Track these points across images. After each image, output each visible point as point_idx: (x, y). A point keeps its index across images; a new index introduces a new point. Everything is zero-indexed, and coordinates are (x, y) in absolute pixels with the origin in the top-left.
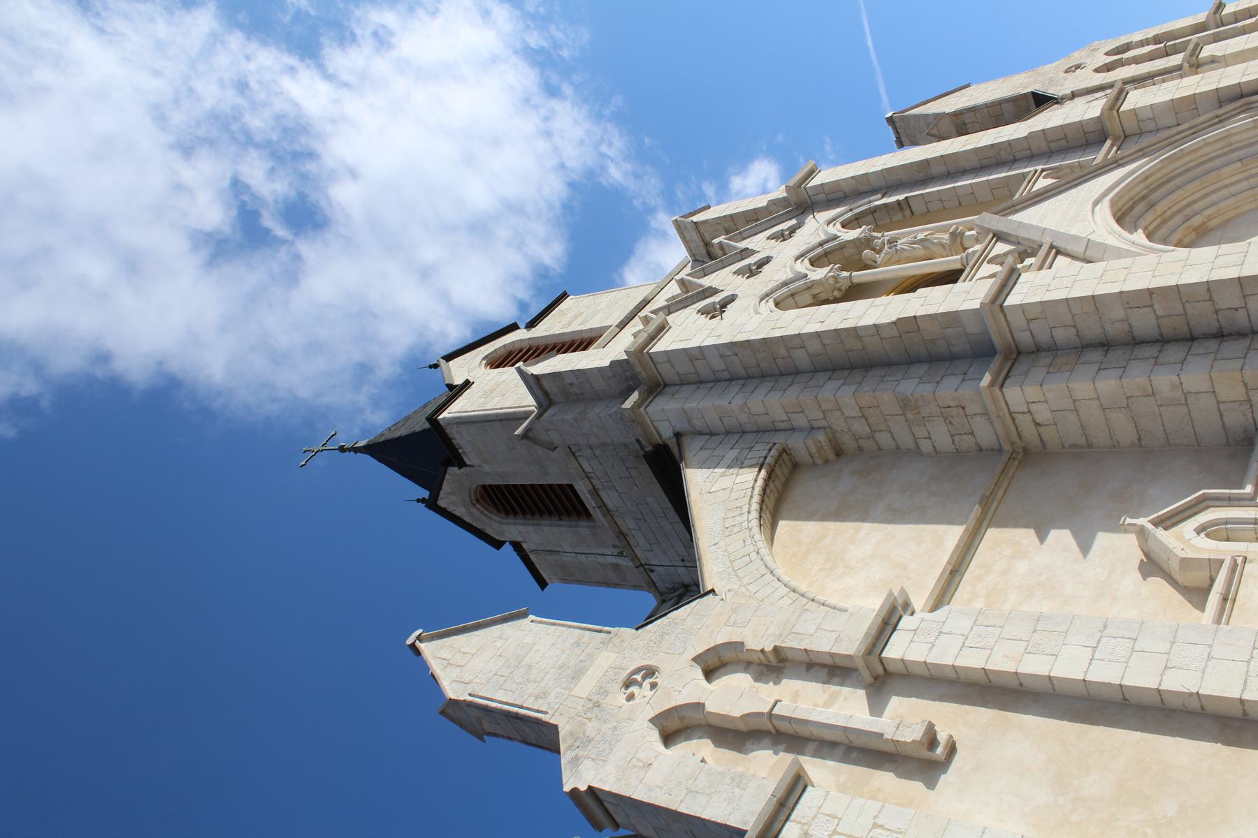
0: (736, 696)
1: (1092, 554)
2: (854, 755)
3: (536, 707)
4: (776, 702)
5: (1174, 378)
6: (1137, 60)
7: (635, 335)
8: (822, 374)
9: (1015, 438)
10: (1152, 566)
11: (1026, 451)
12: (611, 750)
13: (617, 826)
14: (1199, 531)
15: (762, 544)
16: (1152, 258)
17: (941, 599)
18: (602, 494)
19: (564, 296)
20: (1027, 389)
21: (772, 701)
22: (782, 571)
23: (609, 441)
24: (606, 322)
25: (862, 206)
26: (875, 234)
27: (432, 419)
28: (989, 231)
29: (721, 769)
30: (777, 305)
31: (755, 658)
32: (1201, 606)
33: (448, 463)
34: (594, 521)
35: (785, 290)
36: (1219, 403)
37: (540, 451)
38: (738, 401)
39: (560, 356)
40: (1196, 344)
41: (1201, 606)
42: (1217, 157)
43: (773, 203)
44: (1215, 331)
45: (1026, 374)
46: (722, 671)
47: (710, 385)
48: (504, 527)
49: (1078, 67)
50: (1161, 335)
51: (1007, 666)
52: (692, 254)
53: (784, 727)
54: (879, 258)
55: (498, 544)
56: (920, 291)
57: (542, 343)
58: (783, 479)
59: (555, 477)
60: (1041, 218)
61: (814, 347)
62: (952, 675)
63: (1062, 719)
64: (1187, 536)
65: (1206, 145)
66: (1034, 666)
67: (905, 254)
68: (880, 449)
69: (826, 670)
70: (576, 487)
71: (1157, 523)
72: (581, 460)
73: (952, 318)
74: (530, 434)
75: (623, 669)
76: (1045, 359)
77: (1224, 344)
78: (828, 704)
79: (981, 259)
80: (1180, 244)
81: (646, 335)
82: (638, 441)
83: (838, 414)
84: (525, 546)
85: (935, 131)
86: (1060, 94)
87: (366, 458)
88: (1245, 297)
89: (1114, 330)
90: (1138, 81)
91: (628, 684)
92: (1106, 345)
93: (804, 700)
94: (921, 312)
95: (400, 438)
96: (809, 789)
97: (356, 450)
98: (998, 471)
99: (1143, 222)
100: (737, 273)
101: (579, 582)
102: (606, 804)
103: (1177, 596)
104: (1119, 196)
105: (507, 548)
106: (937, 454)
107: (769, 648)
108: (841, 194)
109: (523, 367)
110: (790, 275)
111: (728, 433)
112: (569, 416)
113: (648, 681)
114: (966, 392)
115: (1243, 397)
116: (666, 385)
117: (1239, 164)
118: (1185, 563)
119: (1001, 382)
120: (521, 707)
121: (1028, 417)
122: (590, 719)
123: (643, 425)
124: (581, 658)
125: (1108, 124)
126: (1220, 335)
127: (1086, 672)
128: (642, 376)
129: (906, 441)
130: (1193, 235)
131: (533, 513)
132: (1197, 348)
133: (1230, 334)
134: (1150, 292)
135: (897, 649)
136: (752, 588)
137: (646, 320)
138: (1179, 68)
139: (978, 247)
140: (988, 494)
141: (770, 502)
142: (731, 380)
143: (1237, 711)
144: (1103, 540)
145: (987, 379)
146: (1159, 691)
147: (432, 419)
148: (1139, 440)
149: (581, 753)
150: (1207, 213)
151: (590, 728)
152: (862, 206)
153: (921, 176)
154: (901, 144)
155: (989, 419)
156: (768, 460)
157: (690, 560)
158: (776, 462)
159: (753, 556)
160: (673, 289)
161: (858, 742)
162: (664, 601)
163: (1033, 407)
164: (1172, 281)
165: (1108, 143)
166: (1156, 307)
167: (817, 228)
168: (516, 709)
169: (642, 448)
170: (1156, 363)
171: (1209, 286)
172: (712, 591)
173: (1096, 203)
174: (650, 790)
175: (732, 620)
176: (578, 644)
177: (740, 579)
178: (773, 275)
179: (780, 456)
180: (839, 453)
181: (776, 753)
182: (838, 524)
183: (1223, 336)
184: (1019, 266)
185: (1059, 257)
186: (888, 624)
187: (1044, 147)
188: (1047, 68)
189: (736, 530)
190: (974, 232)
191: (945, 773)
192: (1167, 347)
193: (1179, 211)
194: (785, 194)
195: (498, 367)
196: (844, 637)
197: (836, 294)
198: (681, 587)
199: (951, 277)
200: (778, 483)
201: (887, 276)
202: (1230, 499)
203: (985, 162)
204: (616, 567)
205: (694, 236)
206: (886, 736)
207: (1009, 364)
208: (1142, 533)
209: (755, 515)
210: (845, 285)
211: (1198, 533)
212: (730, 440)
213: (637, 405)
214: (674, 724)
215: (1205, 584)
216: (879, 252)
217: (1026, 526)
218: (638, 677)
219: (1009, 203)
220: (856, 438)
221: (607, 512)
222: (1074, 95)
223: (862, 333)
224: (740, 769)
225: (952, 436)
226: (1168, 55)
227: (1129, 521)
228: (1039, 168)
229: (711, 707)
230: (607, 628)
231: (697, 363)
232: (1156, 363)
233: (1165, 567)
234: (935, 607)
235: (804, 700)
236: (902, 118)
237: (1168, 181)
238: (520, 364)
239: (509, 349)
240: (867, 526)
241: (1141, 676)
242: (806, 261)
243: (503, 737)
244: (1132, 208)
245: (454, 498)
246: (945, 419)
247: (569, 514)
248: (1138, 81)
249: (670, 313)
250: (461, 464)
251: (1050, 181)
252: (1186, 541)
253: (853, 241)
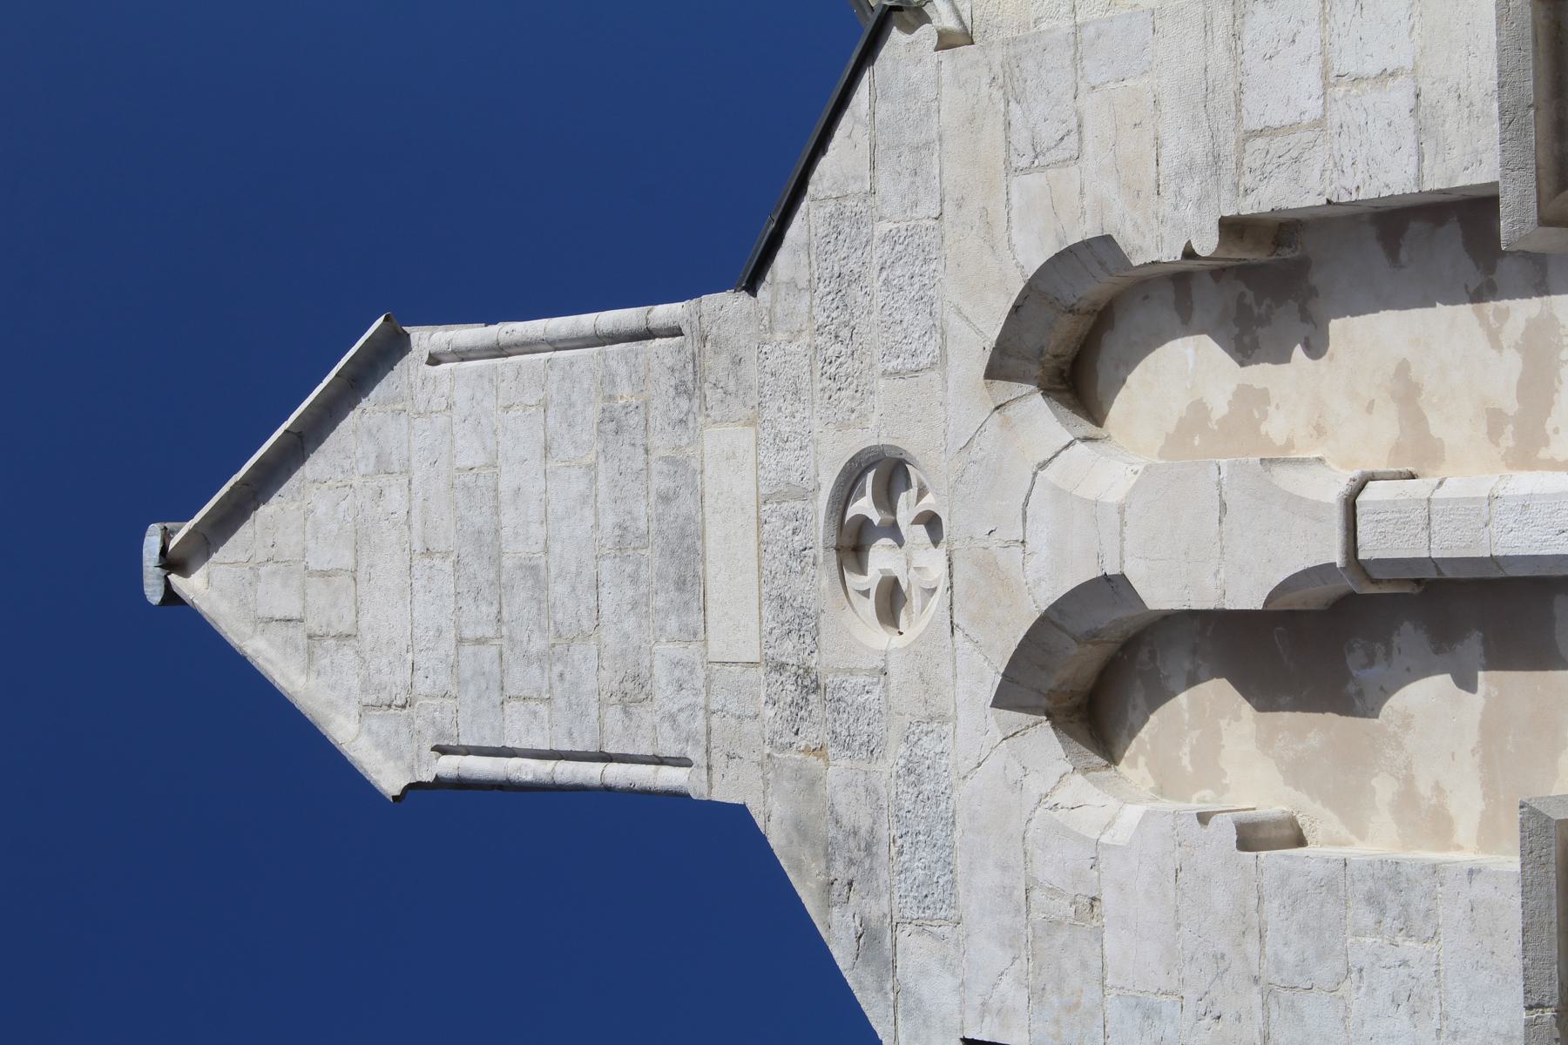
0: (1212, 477)
4: (1350, 506)
46: (1112, 345)
149: (876, 909)
175: (1021, 139)
218: (864, 506)
230: (663, 313)
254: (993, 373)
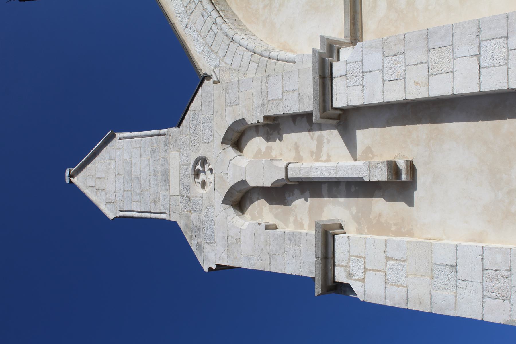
46: (244, 138)
63: (477, 120)
91: (197, 174)
124: (161, 162)
136: (228, 60)
149: (200, 240)
175: (228, 101)
191: (415, 190)
218: (199, 167)
254: (222, 143)
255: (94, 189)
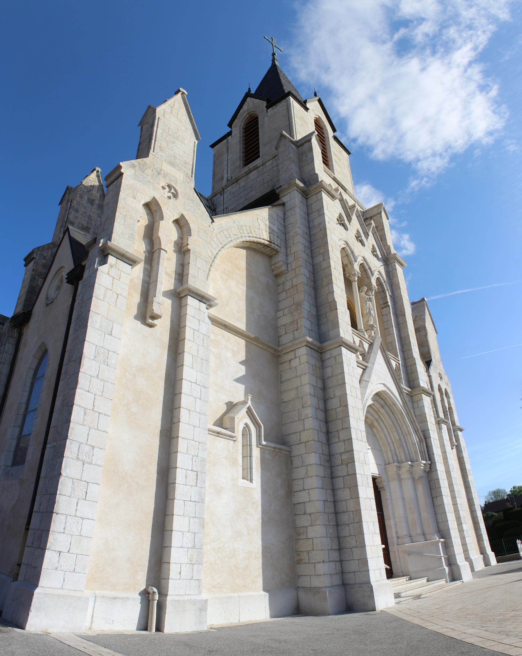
0: (168, 234)
1: (235, 383)
2: (146, 285)
3: (156, 147)
5: (310, 415)
6: (442, 400)
7: (330, 185)
8: (312, 269)
9: (284, 352)
10: (231, 406)
11: (279, 356)
12: (140, 181)
13: (108, 187)
14: (246, 424)
15: (235, 243)
16: (360, 406)
17: (216, 322)
18: (256, 171)
19: (349, 153)
20: (305, 357)
21: (166, 249)
22: (224, 250)
23: (280, 173)
24: (337, 171)
25: (386, 286)
26: (374, 292)
27: (289, 94)
28: (374, 341)
29: (136, 229)
30: (343, 248)
31: (185, 241)
32: (215, 424)
33: (268, 101)
34: (243, 167)
35: (350, 252)
36: (300, 432)
37: (275, 143)
38: (299, 231)
39: (320, 151)
40: (324, 424)
41: (215, 424)
42: (402, 431)
43: (389, 247)
44: (330, 430)
45: (312, 356)
46: (178, 227)
47: (307, 219)
48: (238, 128)
49: (441, 378)
50: (328, 410)
51: (186, 349)
52: (366, 211)
53: (156, 255)
54: (363, 294)
55: (230, 125)
56: (348, 311)
57: (326, 143)
58: (264, 251)
59: (263, 150)
60: (379, 362)
61: (324, 265)
62: (182, 326)
64: (244, 420)
65: (407, 427)
66: (187, 359)
67: (365, 305)
68: (279, 294)
69: (181, 272)
70: (259, 159)
71: (249, 408)
72: (271, 161)
73: (336, 325)
74: (283, 138)
75: (176, 184)
76: (318, 364)
77: (324, 434)
78: (166, 273)
79: (362, 338)
80: (366, 417)
81: (330, 190)
82: (281, 186)
83: (294, 275)
84: (230, 137)
85: (418, 319)
86: (430, 371)
87: (270, 65)
88: (344, 441)
89: (331, 392)
90: (434, 401)
91: (169, 186)
92: (324, 389)
93: (168, 263)
94: (339, 311)
95: (280, 80)
96: (130, 267)
97: (273, 60)
98: (270, 344)
99: (376, 403)
100: (358, 231)
101: (214, 162)
102: (116, 181)
103: (219, 416)
104: (387, 394)
105: (229, 129)
106: (277, 319)
107: (189, 247)
108: (391, 278)
109: (315, 134)
110: (356, 255)
111: (285, 227)
112: (292, 155)
113: (171, 195)
114: (304, 331)
115: (302, 440)
116: (307, 199)
117: (398, 439)
118: (233, 419)
119: (309, 345)
120: (155, 141)
121: (294, 357)
122: (152, 171)
123: (288, 188)
124: (180, 165)
125: (417, 389)
126: (328, 433)
127: (186, 380)
128: (311, 187)
129: (282, 305)
130: (370, 423)
131: (245, 140)
132: (323, 424)
133: (328, 436)
134: (346, 406)
135: (191, 301)
136: (215, 239)
137: (337, 190)
138: (438, 417)
139: (367, 336)
140: (260, 340)
141: (254, 246)
142: (309, 228)
143: (174, 435)
144: (241, 388)
145: (310, 339)
146: (180, 407)
147: (289, 94)
148: (284, 402)
149: (137, 168)
150: (379, 428)
151: (149, 171)
152: (386, 286)
153: (398, 313)
154: (413, 304)
155: (292, 341)
156: (273, 245)
157: (227, 211)
158: (272, 248)
159: (230, 239)
160: (351, 202)
161: (151, 286)
162: (207, 200)
163: (298, 359)
164: (351, 414)
165: (409, 390)
166: (340, 408)
167: (377, 267)
168: (154, 138)
169: (278, 188)
170: (316, 408)
171: (349, 428)
172: (213, 221)
173: (384, 385)
174: (124, 199)
175: (201, 230)
176: (186, 163)
177: (219, 233)
178: (356, 247)
179: (275, 250)
180: (277, 276)
181: (144, 252)
182: (245, 276)
183: (328, 433)
184: (358, 353)
185: (362, 370)
186: (202, 298)
187: (409, 364)
188: (441, 366)
189: (241, 231)
190: (373, 334)
192: (323, 412)
193: (380, 417)
194: (392, 253)
195: (315, 123)
196: (195, 280)
197: (348, 275)
198: (214, 208)
199: (354, 325)
200: (262, 249)
201: (355, 297)
202: (259, 436)
203: (403, 340)
204: (222, 178)
205: (375, 212)
206: (155, 298)
207: (317, 349)
208: (245, 403)
209: (248, 239)
210: (352, 278)
211: (245, 424)
212: (282, 228)
213: (297, 186)
214: (153, 207)
215: (224, 426)
216: (366, 293)
217: (246, 356)
218: (173, 191)
219: (385, 350)
220: (283, 284)
221: (247, 174)
222: (429, 376)
223: (330, 286)
224: (136, 237)
225: (285, 325)
226: (444, 412)
227: (250, 398)
228: (400, 362)
229: (162, 223)
231: (317, 213)
232: (316, 408)
233: (231, 412)
234: (210, 318)
235: (168, 263)
236: (424, 304)
237: (393, 413)
238: (317, 133)
239: (324, 128)
240: (245, 288)
241: (186, 400)
242: (362, 262)
243: (141, 134)
244: (382, 399)
245: (251, 104)
246: (292, 322)
247: (246, 156)
248: (434, 401)
249: (340, 201)
250: (268, 107)
251: (394, 366)
252: (242, 419)
253: (371, 282)
254: (182, 214)
255: (173, 106)
